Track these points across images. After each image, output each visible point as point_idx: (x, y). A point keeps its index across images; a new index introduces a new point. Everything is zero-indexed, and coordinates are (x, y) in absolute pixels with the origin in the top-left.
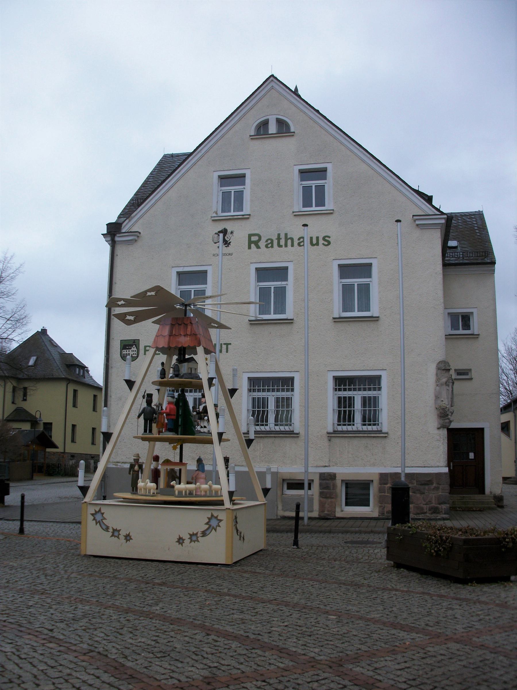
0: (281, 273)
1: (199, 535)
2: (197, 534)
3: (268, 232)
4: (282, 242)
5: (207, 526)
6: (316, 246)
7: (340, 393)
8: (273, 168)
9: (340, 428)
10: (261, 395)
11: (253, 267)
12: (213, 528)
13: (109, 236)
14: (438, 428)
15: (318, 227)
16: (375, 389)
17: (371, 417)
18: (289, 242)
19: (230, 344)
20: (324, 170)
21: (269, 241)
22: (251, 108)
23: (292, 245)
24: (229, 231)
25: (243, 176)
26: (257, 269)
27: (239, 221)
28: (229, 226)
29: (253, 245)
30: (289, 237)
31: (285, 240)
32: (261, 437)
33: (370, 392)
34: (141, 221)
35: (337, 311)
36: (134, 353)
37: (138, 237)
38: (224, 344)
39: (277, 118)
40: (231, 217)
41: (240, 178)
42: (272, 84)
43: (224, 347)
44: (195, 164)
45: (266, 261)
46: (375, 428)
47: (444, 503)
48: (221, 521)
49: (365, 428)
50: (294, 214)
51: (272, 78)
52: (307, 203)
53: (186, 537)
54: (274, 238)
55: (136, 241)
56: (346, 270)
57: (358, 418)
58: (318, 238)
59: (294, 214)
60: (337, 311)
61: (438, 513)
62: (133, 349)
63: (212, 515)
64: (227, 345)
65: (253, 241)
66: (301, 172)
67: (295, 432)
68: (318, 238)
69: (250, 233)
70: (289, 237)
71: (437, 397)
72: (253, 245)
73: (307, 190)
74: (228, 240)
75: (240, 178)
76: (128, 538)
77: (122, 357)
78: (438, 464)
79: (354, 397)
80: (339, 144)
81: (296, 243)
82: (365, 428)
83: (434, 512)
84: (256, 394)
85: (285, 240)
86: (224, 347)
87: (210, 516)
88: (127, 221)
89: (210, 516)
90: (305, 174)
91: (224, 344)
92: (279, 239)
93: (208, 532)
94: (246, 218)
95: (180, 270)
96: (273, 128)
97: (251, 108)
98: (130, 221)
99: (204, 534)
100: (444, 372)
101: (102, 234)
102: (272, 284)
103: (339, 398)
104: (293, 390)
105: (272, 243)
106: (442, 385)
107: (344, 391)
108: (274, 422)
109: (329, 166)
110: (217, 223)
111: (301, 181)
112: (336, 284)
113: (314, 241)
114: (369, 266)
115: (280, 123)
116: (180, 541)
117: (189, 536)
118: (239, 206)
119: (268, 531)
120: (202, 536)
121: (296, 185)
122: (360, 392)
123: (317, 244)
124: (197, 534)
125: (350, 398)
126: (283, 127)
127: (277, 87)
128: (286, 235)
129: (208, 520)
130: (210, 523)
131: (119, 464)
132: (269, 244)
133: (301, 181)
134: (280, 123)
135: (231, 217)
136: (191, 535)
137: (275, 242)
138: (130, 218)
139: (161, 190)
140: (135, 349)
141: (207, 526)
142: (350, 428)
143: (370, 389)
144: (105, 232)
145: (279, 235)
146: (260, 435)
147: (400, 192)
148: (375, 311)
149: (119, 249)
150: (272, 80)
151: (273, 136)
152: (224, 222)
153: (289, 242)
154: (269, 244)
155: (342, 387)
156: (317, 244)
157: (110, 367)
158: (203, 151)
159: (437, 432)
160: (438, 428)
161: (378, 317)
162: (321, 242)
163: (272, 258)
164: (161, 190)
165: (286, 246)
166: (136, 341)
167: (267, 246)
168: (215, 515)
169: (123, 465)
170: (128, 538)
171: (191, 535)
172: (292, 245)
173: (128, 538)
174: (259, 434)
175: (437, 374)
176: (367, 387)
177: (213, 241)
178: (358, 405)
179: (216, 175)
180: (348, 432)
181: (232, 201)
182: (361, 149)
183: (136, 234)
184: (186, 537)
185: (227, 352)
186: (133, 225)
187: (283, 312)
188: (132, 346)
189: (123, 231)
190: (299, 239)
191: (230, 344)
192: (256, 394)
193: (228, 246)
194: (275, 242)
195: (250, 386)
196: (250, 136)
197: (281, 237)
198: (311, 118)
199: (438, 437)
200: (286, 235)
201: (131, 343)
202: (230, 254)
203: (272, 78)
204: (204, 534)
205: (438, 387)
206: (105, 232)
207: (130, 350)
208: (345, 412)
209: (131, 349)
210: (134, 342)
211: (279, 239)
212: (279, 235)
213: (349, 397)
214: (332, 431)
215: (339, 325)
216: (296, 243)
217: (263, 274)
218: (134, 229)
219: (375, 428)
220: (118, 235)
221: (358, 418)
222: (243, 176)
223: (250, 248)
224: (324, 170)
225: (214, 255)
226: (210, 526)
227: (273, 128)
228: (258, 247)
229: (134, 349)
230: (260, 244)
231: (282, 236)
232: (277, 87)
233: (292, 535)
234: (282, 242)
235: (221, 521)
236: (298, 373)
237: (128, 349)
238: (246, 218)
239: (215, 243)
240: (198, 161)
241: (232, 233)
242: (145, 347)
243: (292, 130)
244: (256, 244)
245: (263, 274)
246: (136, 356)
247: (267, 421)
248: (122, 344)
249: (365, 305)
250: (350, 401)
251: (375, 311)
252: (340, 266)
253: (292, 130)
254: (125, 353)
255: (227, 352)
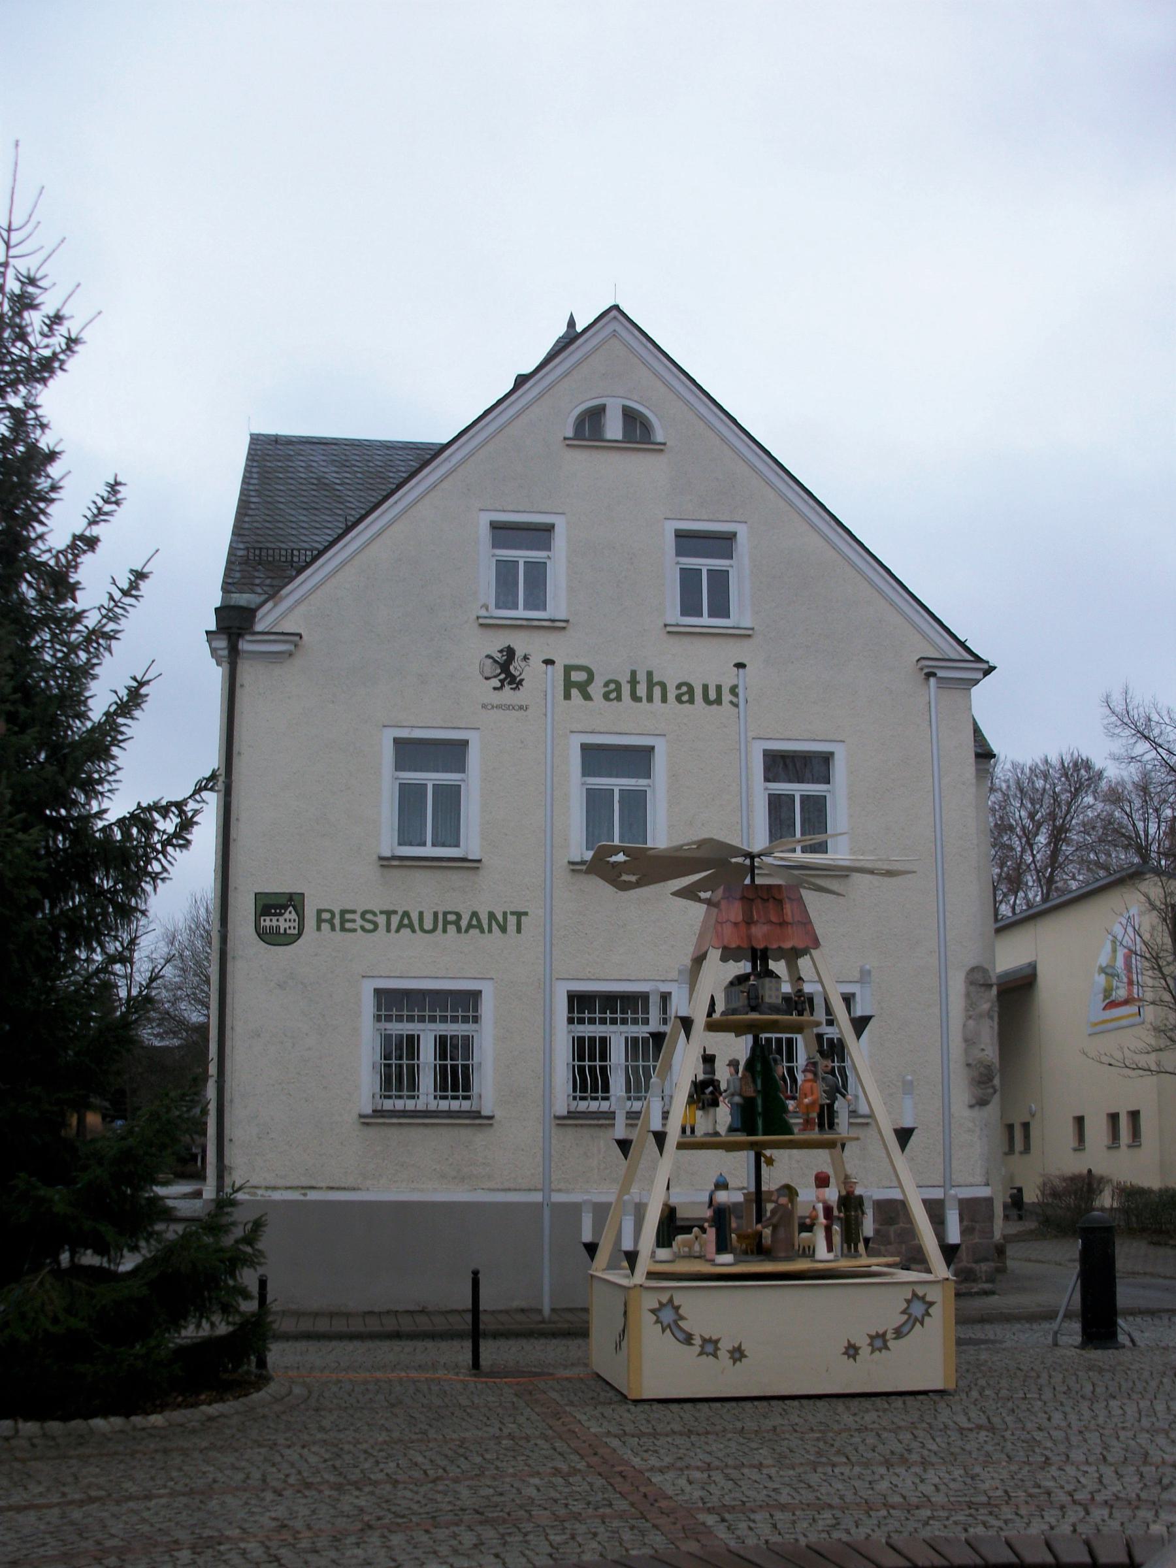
0: (637, 759)
1: (888, 1336)
2: (884, 1334)
3: (610, 665)
4: (642, 690)
5: (906, 1317)
6: (715, 706)
7: (581, 1028)
8: (612, 519)
9: (583, 1106)
10: (597, 1030)
11: (576, 742)
12: (916, 1320)
13: (224, 637)
14: (971, 1106)
15: (706, 664)
16: (466, 1020)
17: (456, 1078)
18: (657, 691)
19: (526, 914)
20: (729, 538)
21: (612, 686)
22: (567, 374)
23: (664, 699)
24: (519, 654)
25: (549, 529)
26: (585, 748)
27: (542, 632)
28: (521, 643)
29: (574, 692)
30: (655, 680)
31: (644, 687)
32: (601, 1126)
33: (454, 1026)
34: (302, 608)
35: (388, 844)
36: (292, 924)
37: (296, 646)
38: (512, 913)
39: (624, 406)
40: (524, 623)
41: (540, 534)
42: (615, 326)
43: (512, 920)
44: (434, 486)
45: (604, 730)
46: (466, 1105)
47: (986, 1260)
48: (931, 1304)
49: (444, 1105)
50: (669, 629)
51: (614, 313)
52: (690, 606)
53: (862, 1342)
54: (624, 679)
55: (291, 654)
56: (410, 752)
57: (427, 1081)
58: (719, 688)
59: (669, 629)
60: (388, 844)
61: (974, 1281)
62: (287, 915)
63: (915, 1295)
64: (519, 915)
65: (577, 683)
66: (680, 535)
67: (484, 1113)
68: (719, 688)
69: (568, 662)
70: (655, 680)
71: (969, 1042)
72: (574, 692)
73: (689, 579)
74: (516, 673)
75: (540, 534)
76: (738, 1354)
77: (259, 935)
78: (971, 1180)
79: (419, 1036)
80: (763, 483)
81: (672, 694)
82: (444, 1105)
83: (966, 1280)
84: (587, 1030)
85: (644, 687)
86: (512, 920)
87: (909, 1296)
88: (269, 605)
89: (909, 1296)
90: (688, 541)
91: (512, 913)
92: (633, 682)
93: (905, 1329)
94: (556, 626)
95: (404, 734)
96: (614, 428)
97: (567, 374)
98: (275, 606)
99: (899, 1333)
100: (983, 989)
101: (995, 668)
102: (431, 778)
103: (387, 1038)
104: (476, 1020)
105: (618, 688)
106: (981, 1016)
107: (611, 1023)
108: (623, 1094)
109: (742, 531)
110: (491, 633)
111: (494, 547)
112: (387, 781)
113: (712, 695)
114: (826, 759)
115: (631, 417)
116: (852, 1351)
117: (869, 1341)
118: (537, 598)
119: (957, 1323)
120: (895, 1339)
121: (670, 566)
122: (433, 1026)
123: (718, 701)
124: (884, 1334)
125: (411, 1038)
126: (637, 428)
127: (624, 333)
128: (650, 674)
129: (905, 1305)
130: (910, 1311)
131: (260, 1192)
132: (683, 694)
133: (494, 547)
134: (631, 417)
135: (524, 623)
136: (872, 1337)
137: (626, 690)
138: (277, 599)
139: (353, 539)
140: (294, 916)
141: (906, 1317)
142: (410, 1105)
143: (454, 1020)
144: (213, 627)
145: (634, 673)
146: (601, 1122)
147: (892, 604)
148: (471, 844)
149: (248, 672)
150: (615, 318)
151: (613, 446)
152: (507, 632)
153: (657, 691)
154: (683, 694)
155: (460, 1013)
156: (718, 701)
157: (229, 957)
158: (454, 461)
159: (967, 1113)
160: (971, 1106)
161: (479, 861)
162: (727, 697)
163: (622, 724)
164: (353, 539)
165: (650, 699)
166: (294, 897)
167: (606, 696)
168: (920, 1294)
169: (269, 1193)
170: (738, 1354)
171: (872, 1337)
172: (664, 699)
173: (737, 1355)
174: (599, 1119)
175: (968, 995)
176: (449, 1014)
177: (482, 672)
178: (427, 1054)
179: (485, 519)
180: (404, 1113)
181: (521, 584)
182: (811, 502)
183: (292, 638)
184: (862, 1342)
185: (519, 930)
186: (284, 615)
187: (821, 848)
188: (285, 907)
189: (259, 627)
190: (679, 687)
191: (526, 914)
192: (587, 1030)
193: (517, 688)
194: (626, 690)
195: (379, 1009)
196: (565, 439)
197: (638, 678)
198: (701, 418)
199: (971, 1125)
200: (650, 674)
201: (283, 901)
202: (521, 708)
203: (614, 313)
204: (899, 1333)
205: (971, 1022)
206: (213, 627)
207: (281, 919)
208: (454, 1068)
209: (281, 914)
210: (291, 899)
211: (633, 682)
212: (634, 673)
213: (600, 1038)
214: (369, 1111)
215: (396, 873)
216: (672, 694)
217: (597, 758)
218: (288, 626)
219: (466, 1105)
220: (248, 638)
221: (427, 1081)
222: (549, 529)
223: (567, 696)
224: (729, 538)
225: (484, 706)
226: (910, 1315)
227: (614, 428)
228: (587, 697)
229: (291, 915)
230: (591, 689)
231: (642, 677)
232: (624, 333)
233: (468, 1344)
234: (642, 690)
235: (931, 1304)
236: (490, 983)
237: (275, 915)
238: (556, 626)
239: (487, 678)
240: (442, 480)
241: (526, 658)
242: (319, 912)
243: (659, 436)
244: (583, 688)
245: (597, 758)
246: (296, 932)
247: (606, 1088)
248: (260, 903)
249: (449, 832)
250: (411, 1044)
251: (471, 844)
252: (585, 748)
253: (660, 439)
254: (268, 923)
255: (519, 930)
